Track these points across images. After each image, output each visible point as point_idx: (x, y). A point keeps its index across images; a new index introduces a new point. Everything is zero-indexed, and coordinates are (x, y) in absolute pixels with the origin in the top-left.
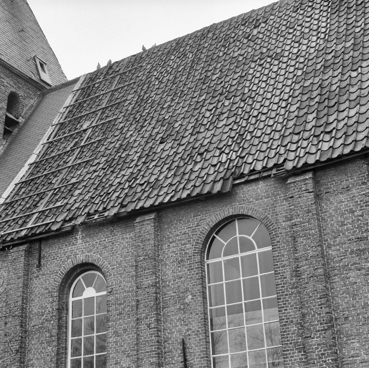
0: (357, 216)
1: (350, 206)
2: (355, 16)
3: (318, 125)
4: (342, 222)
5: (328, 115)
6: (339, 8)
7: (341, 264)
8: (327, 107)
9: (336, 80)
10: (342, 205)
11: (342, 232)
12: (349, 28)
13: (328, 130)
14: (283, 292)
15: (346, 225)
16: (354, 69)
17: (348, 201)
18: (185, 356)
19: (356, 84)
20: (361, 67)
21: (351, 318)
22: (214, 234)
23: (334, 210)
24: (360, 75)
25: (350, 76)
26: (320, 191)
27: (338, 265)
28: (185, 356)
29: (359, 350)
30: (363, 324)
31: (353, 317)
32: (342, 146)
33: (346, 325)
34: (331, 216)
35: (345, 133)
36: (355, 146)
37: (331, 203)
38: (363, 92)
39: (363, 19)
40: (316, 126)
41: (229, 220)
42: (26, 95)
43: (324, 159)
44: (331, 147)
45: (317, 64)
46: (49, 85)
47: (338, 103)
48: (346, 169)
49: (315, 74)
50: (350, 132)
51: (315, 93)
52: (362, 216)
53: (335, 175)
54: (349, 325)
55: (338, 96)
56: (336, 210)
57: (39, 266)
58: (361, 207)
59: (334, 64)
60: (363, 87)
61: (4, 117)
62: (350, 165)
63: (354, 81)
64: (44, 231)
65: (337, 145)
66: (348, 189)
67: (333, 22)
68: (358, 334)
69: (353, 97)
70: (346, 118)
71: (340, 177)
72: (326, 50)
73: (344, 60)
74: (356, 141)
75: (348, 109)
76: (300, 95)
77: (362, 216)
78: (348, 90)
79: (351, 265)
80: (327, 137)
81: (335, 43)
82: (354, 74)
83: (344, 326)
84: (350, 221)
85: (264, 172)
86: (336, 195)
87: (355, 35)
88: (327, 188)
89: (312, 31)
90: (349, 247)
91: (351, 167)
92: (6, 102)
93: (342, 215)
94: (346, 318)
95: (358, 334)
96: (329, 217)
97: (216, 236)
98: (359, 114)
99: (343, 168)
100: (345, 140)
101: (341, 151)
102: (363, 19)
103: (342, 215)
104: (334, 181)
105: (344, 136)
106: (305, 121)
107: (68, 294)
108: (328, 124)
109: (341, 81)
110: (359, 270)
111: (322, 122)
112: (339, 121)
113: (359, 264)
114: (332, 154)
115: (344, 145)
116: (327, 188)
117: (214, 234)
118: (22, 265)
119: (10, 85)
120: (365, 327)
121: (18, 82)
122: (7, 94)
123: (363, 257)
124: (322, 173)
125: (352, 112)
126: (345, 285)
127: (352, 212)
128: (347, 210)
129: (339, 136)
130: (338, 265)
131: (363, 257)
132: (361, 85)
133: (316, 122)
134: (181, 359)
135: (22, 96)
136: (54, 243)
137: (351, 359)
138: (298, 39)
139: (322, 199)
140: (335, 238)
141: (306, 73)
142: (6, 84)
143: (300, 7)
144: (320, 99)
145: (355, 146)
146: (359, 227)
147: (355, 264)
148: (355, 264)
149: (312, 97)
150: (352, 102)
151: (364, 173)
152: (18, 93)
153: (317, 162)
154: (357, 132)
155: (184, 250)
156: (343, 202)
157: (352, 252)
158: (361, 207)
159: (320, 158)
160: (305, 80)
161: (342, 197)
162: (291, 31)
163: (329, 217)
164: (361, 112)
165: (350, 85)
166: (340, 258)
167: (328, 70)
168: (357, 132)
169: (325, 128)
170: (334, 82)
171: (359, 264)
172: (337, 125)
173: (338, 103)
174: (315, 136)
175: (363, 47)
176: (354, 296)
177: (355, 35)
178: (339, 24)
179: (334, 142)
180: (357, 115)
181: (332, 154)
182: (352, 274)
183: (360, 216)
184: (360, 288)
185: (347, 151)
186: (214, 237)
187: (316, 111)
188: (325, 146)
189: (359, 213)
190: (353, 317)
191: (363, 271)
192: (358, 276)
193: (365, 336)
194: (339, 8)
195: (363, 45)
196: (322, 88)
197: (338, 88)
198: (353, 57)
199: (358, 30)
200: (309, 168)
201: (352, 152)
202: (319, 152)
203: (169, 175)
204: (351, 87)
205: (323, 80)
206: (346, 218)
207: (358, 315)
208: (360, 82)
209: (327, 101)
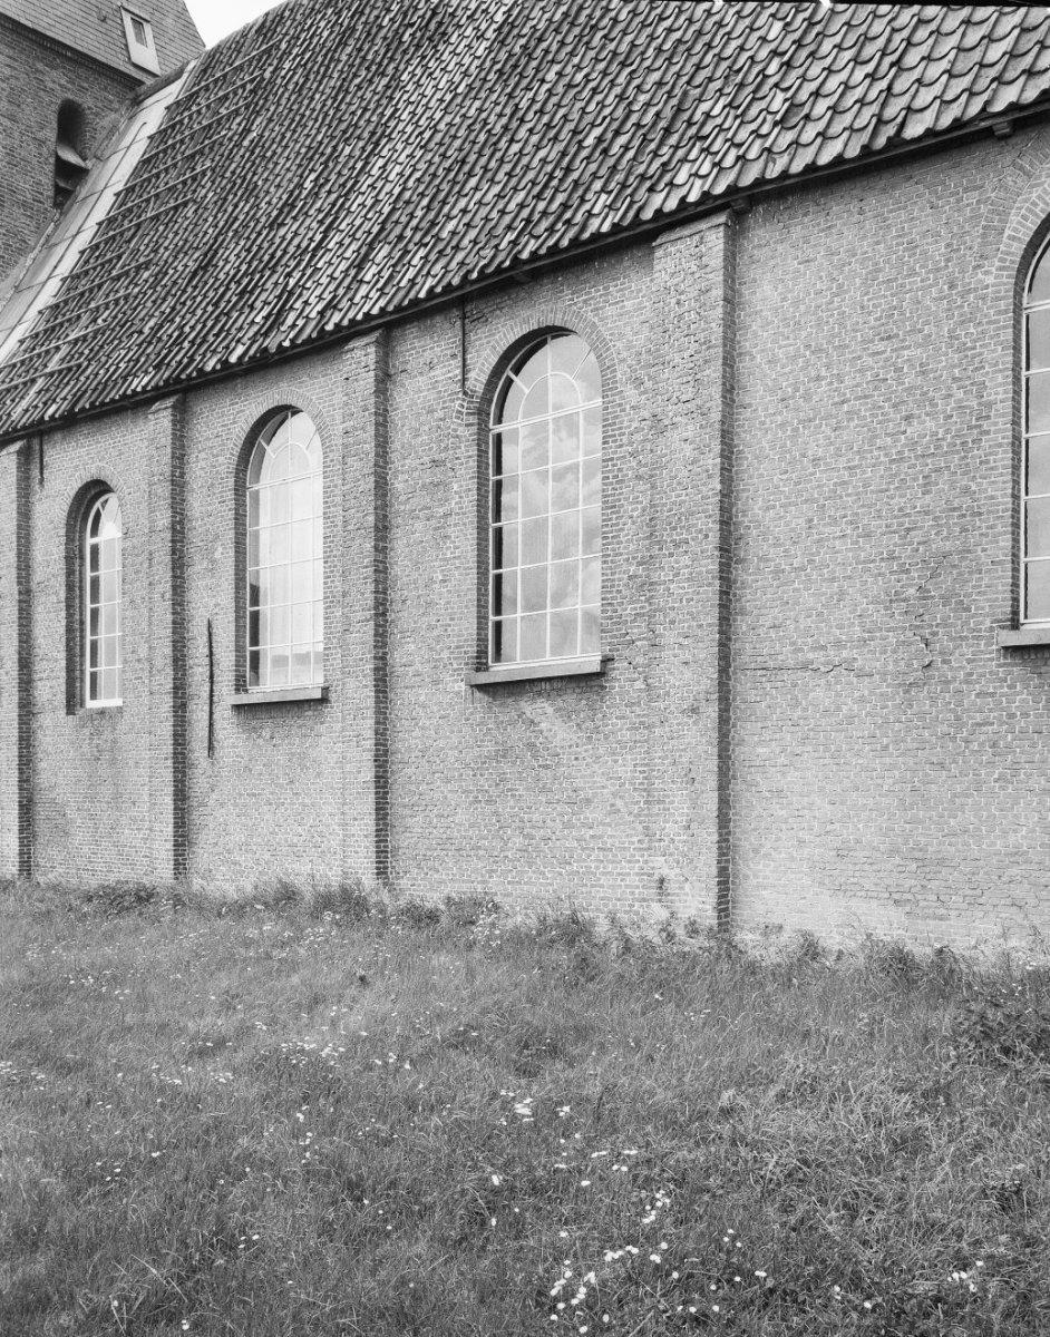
18: (211, 647)
22: (509, 372)
28: (211, 647)
41: (534, 341)
42: (100, 105)
46: (155, 75)
57: (42, 481)
61: (52, 160)
64: (406, 302)
85: (983, 120)
92: (55, 125)
97: (513, 376)
107: (83, 531)
117: (509, 372)
118: (14, 479)
119: (59, 84)
121: (79, 77)
122: (55, 108)
130: (402, 508)
134: (206, 651)
135: (89, 108)
136: (893, 187)
142: (50, 85)
152: (80, 101)
155: (214, 466)
182: (419, 525)
186: (510, 382)
189: (440, 414)
200: (373, 323)
203: (872, 95)
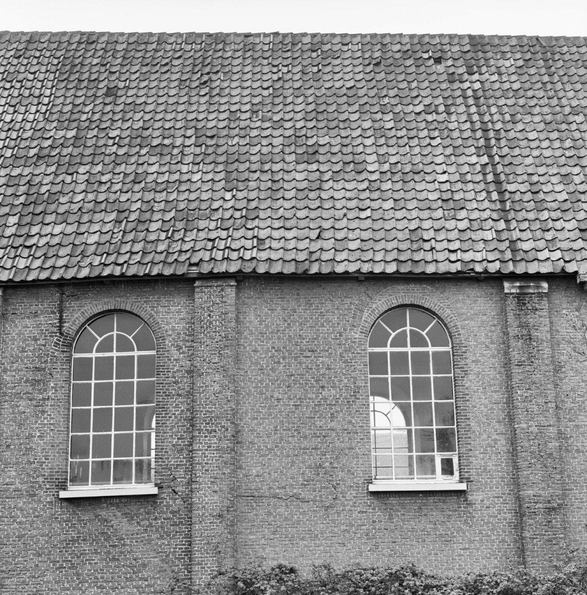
0: (39, 345)
1: (34, 333)
2: (84, 97)
3: (18, 234)
4: (23, 348)
5: (31, 224)
6: (69, 76)
7: (14, 391)
8: (31, 215)
9: (47, 180)
10: (26, 331)
11: (21, 358)
12: (75, 111)
13: (28, 244)
14: (361, 420)
15: (27, 352)
16: (70, 172)
17: (33, 327)
19: (67, 194)
20: (77, 173)
21: (12, 447)
23: (17, 334)
24: (74, 184)
25: (63, 181)
26: (6, 310)
27: (10, 391)
29: (15, 479)
30: (24, 454)
31: (15, 445)
32: (39, 269)
33: (7, 453)
34: (13, 339)
35: (45, 254)
36: (52, 273)
37: (16, 326)
38: (73, 206)
39: (92, 104)
40: (15, 235)
43: (17, 279)
44: (27, 267)
45: (30, 148)
47: (44, 213)
48: (38, 293)
49: (25, 163)
50: (50, 254)
51: (22, 189)
52: (44, 346)
53: (25, 297)
54: (9, 453)
55: (45, 203)
56: (19, 334)
58: (46, 336)
59: (49, 156)
60: (75, 201)
62: (43, 290)
63: (67, 189)
65: (34, 266)
66: (36, 315)
67: (58, 94)
68: (17, 463)
69: (62, 209)
70: (49, 236)
71: (30, 301)
72: (44, 133)
73: (61, 156)
74: (54, 267)
75: (53, 224)
76: (4, 187)
77: (44, 346)
78: (58, 200)
79: (24, 394)
80: (26, 253)
81: (55, 127)
82: (68, 179)
83: (4, 453)
84: (32, 348)
86: (22, 318)
87: (79, 125)
88: (14, 309)
89: (31, 97)
90: (25, 375)
91: (43, 292)
93: (25, 340)
94: (8, 446)
95: (17, 463)
96: (10, 340)
98: (64, 234)
99: (35, 291)
100: (43, 262)
101: (37, 275)
102: (92, 104)
103: (25, 340)
104: (24, 303)
105: (43, 257)
106: (5, 224)
108: (29, 236)
109: (53, 183)
110: (31, 400)
111: (24, 231)
112: (41, 236)
113: (32, 394)
114: (27, 275)
115: (41, 268)
116: (14, 309)
120: (25, 457)
123: (37, 387)
124: (12, 291)
125: (58, 229)
126: (13, 413)
127: (36, 340)
128: (30, 337)
129: (38, 254)
130: (10, 391)
131: (37, 387)
132: (72, 198)
133: (17, 229)
137: (5, 486)
138: (13, 102)
139: (7, 319)
140: (13, 363)
141: (16, 157)
143: (24, 53)
144: (26, 200)
145: (52, 273)
146: (39, 357)
147: (27, 393)
148: (27, 393)
149: (17, 194)
150: (59, 216)
151: (55, 302)
153: (10, 280)
154: (57, 256)
156: (29, 327)
157: (27, 381)
158: (46, 336)
159: (14, 276)
160: (13, 167)
161: (27, 322)
162: (8, 85)
163: (10, 340)
164: (65, 233)
165: (60, 192)
166: (13, 385)
167: (41, 162)
168: (57, 256)
169: (25, 240)
170: (45, 182)
171: (32, 394)
172: (38, 241)
173: (44, 213)
174: (13, 247)
175: (85, 146)
176: (20, 425)
177: (79, 125)
178: (65, 100)
179: (32, 261)
180: (62, 235)
181: (27, 275)
182: (22, 403)
183: (43, 345)
184: (27, 418)
185: (44, 276)
187: (19, 215)
188: (22, 263)
189: (41, 342)
190: (15, 445)
191: (34, 402)
192: (28, 407)
193: (24, 465)
194: (69, 76)
195: (85, 142)
196: (31, 185)
197: (47, 193)
198: (71, 155)
199: (84, 117)
201: (48, 279)
202: (14, 269)
204: (61, 195)
205: (33, 175)
206: (28, 345)
207: (21, 444)
208: (72, 193)
209: (32, 205)
